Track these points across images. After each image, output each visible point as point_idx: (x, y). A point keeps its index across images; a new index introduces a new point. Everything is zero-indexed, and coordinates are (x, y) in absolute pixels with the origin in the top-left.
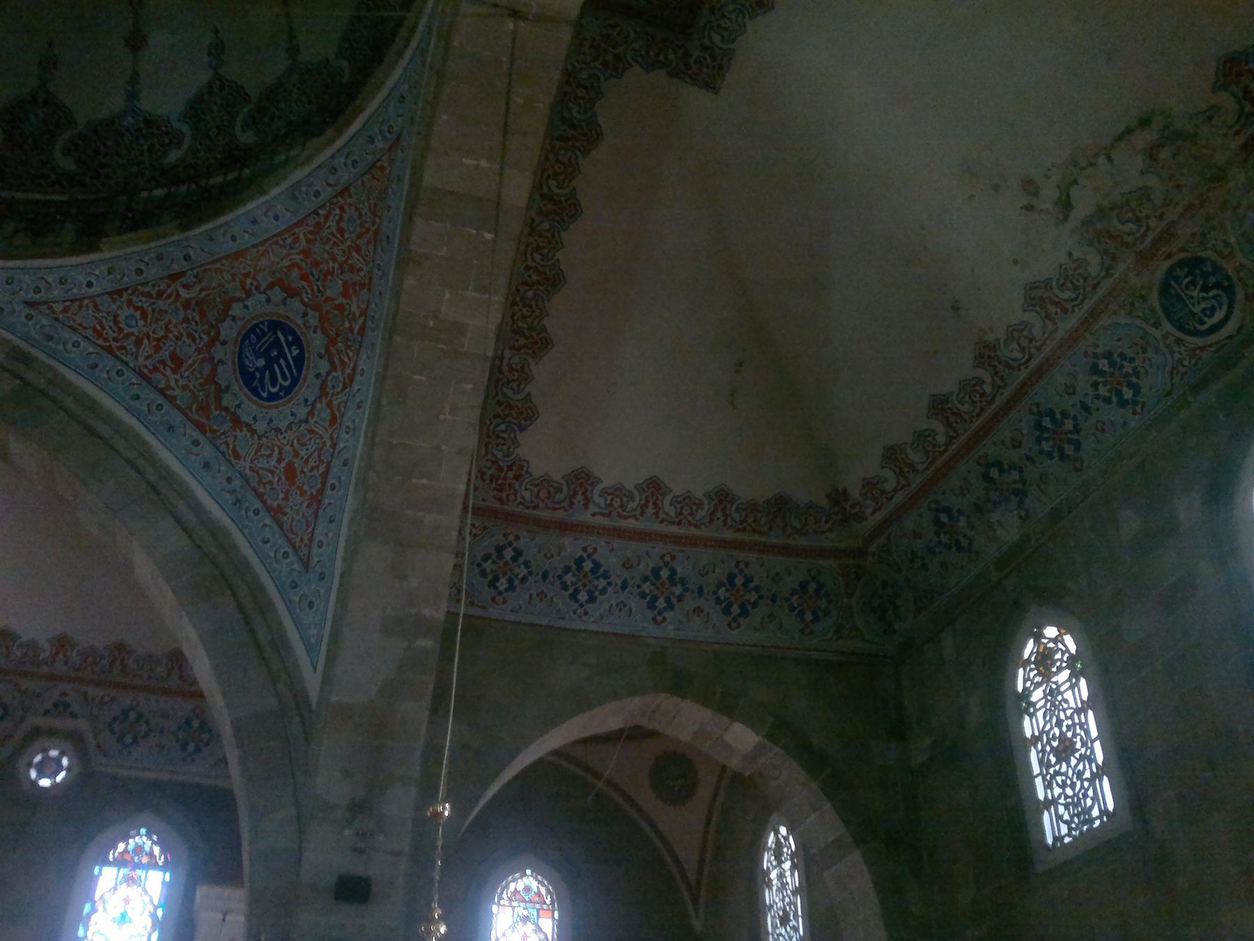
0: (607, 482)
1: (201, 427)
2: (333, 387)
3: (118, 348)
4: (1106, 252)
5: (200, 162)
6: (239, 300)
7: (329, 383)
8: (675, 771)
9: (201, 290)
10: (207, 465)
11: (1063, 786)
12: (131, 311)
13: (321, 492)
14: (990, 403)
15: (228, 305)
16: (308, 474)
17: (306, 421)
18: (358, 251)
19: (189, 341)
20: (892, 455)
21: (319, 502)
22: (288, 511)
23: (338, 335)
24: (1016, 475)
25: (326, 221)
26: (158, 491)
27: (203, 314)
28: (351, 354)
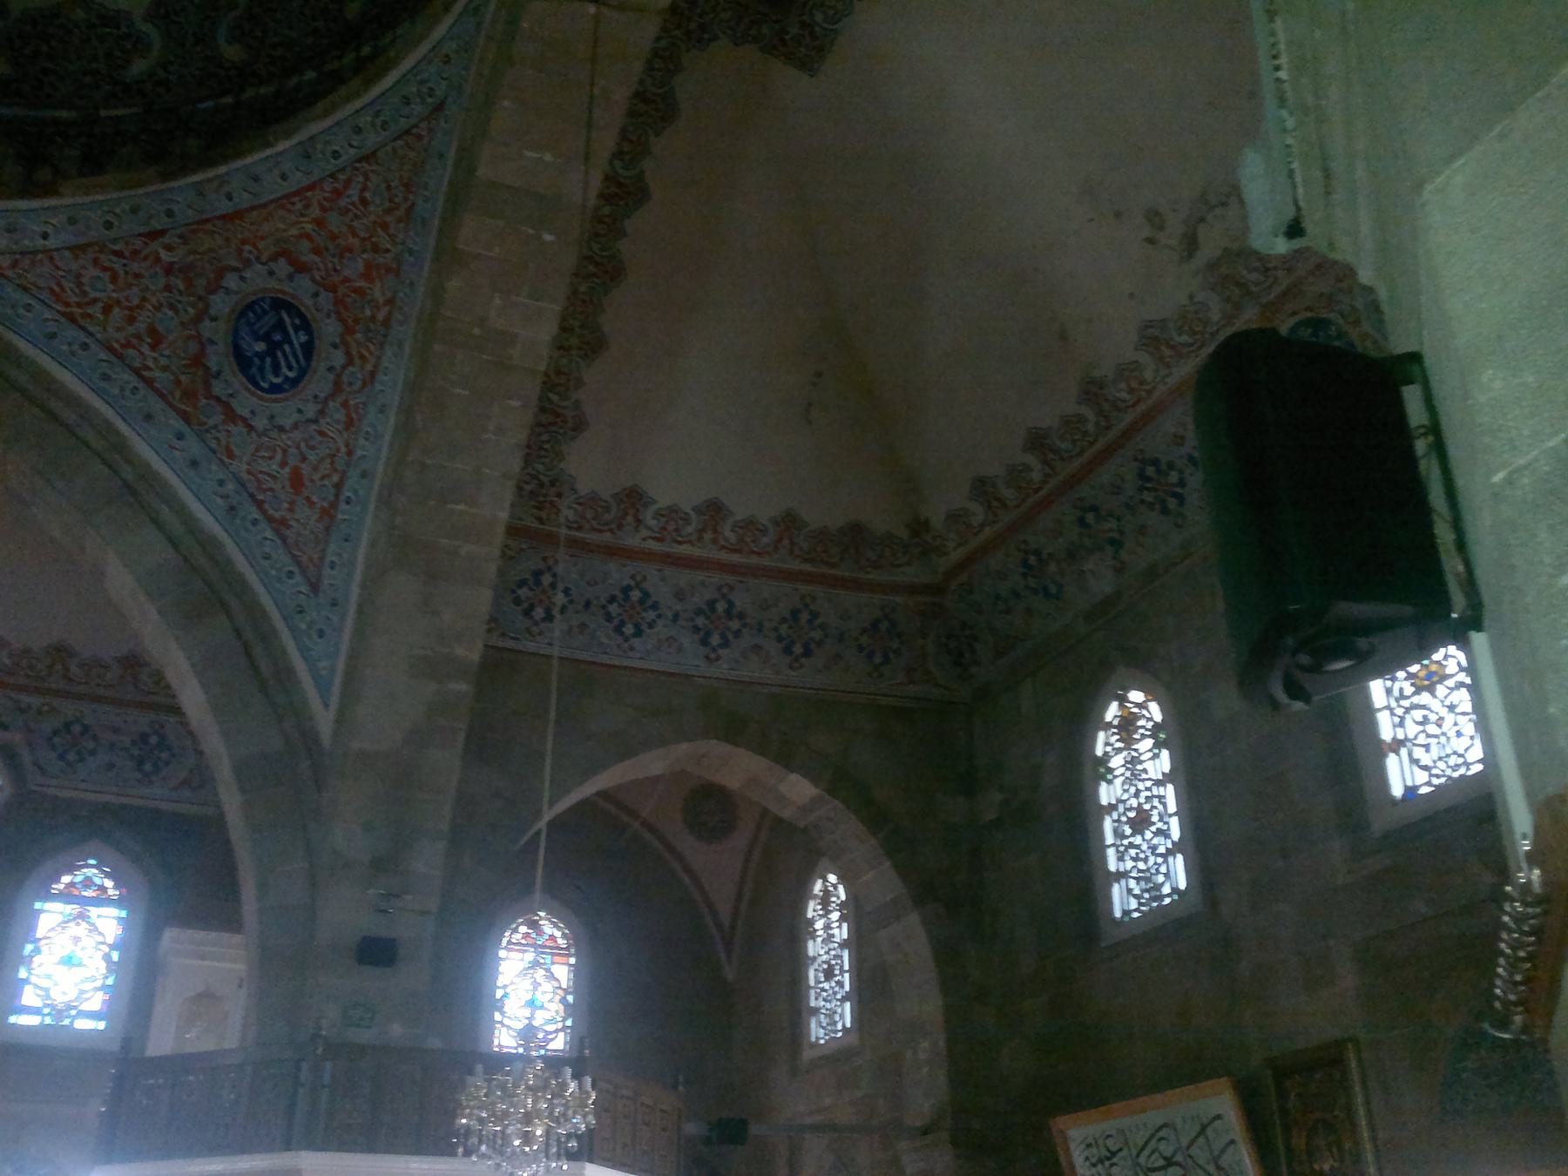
0: (663, 502)
1: (186, 417)
4: (1228, 300)
6: (235, 269)
7: (345, 379)
8: (710, 808)
10: (194, 464)
11: (1135, 859)
12: (96, 272)
14: (1091, 444)
15: (220, 273)
16: (319, 483)
18: (385, 226)
19: (170, 313)
20: (982, 488)
21: (332, 517)
24: (1113, 524)
25: (345, 188)
26: (136, 493)
27: (189, 283)
28: (372, 347)
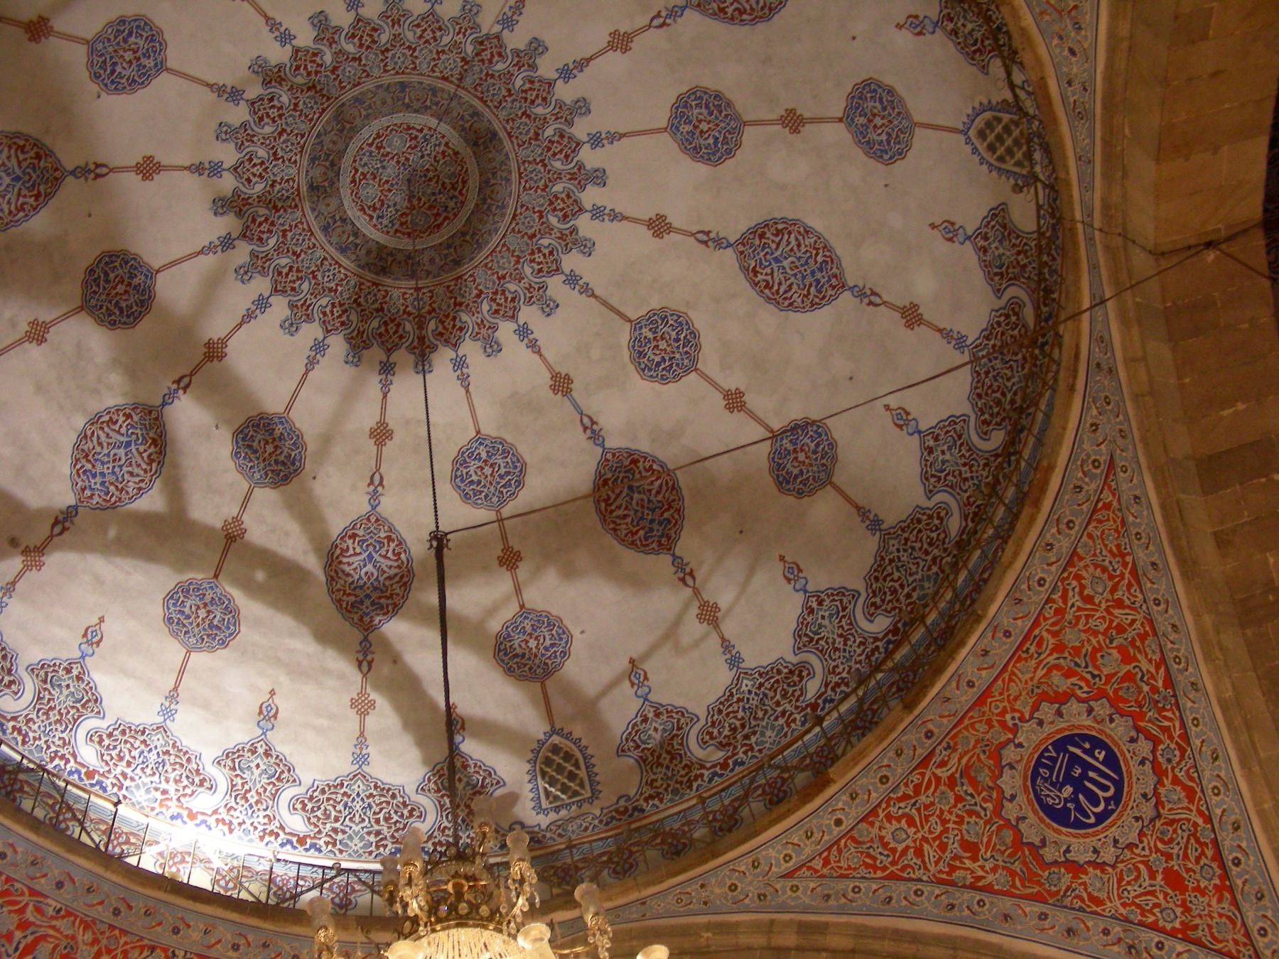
1: (1038, 898)
2: (1169, 760)
3: (902, 870)
5: (844, 675)
9: (959, 760)
12: (895, 824)
13: (1225, 875)
16: (1197, 868)
17: (1159, 816)
18: (1119, 604)
21: (1231, 890)
22: (1197, 921)
23: (1141, 706)
25: (1065, 602)
27: (974, 782)
28: (1169, 714)
